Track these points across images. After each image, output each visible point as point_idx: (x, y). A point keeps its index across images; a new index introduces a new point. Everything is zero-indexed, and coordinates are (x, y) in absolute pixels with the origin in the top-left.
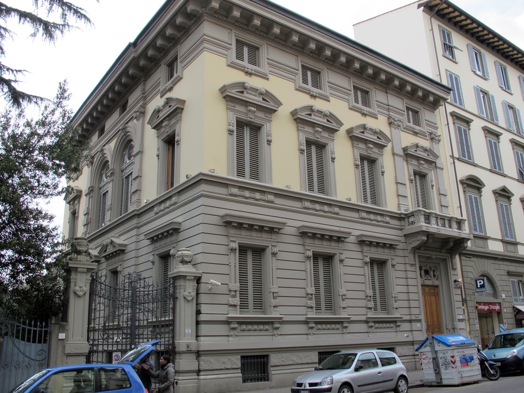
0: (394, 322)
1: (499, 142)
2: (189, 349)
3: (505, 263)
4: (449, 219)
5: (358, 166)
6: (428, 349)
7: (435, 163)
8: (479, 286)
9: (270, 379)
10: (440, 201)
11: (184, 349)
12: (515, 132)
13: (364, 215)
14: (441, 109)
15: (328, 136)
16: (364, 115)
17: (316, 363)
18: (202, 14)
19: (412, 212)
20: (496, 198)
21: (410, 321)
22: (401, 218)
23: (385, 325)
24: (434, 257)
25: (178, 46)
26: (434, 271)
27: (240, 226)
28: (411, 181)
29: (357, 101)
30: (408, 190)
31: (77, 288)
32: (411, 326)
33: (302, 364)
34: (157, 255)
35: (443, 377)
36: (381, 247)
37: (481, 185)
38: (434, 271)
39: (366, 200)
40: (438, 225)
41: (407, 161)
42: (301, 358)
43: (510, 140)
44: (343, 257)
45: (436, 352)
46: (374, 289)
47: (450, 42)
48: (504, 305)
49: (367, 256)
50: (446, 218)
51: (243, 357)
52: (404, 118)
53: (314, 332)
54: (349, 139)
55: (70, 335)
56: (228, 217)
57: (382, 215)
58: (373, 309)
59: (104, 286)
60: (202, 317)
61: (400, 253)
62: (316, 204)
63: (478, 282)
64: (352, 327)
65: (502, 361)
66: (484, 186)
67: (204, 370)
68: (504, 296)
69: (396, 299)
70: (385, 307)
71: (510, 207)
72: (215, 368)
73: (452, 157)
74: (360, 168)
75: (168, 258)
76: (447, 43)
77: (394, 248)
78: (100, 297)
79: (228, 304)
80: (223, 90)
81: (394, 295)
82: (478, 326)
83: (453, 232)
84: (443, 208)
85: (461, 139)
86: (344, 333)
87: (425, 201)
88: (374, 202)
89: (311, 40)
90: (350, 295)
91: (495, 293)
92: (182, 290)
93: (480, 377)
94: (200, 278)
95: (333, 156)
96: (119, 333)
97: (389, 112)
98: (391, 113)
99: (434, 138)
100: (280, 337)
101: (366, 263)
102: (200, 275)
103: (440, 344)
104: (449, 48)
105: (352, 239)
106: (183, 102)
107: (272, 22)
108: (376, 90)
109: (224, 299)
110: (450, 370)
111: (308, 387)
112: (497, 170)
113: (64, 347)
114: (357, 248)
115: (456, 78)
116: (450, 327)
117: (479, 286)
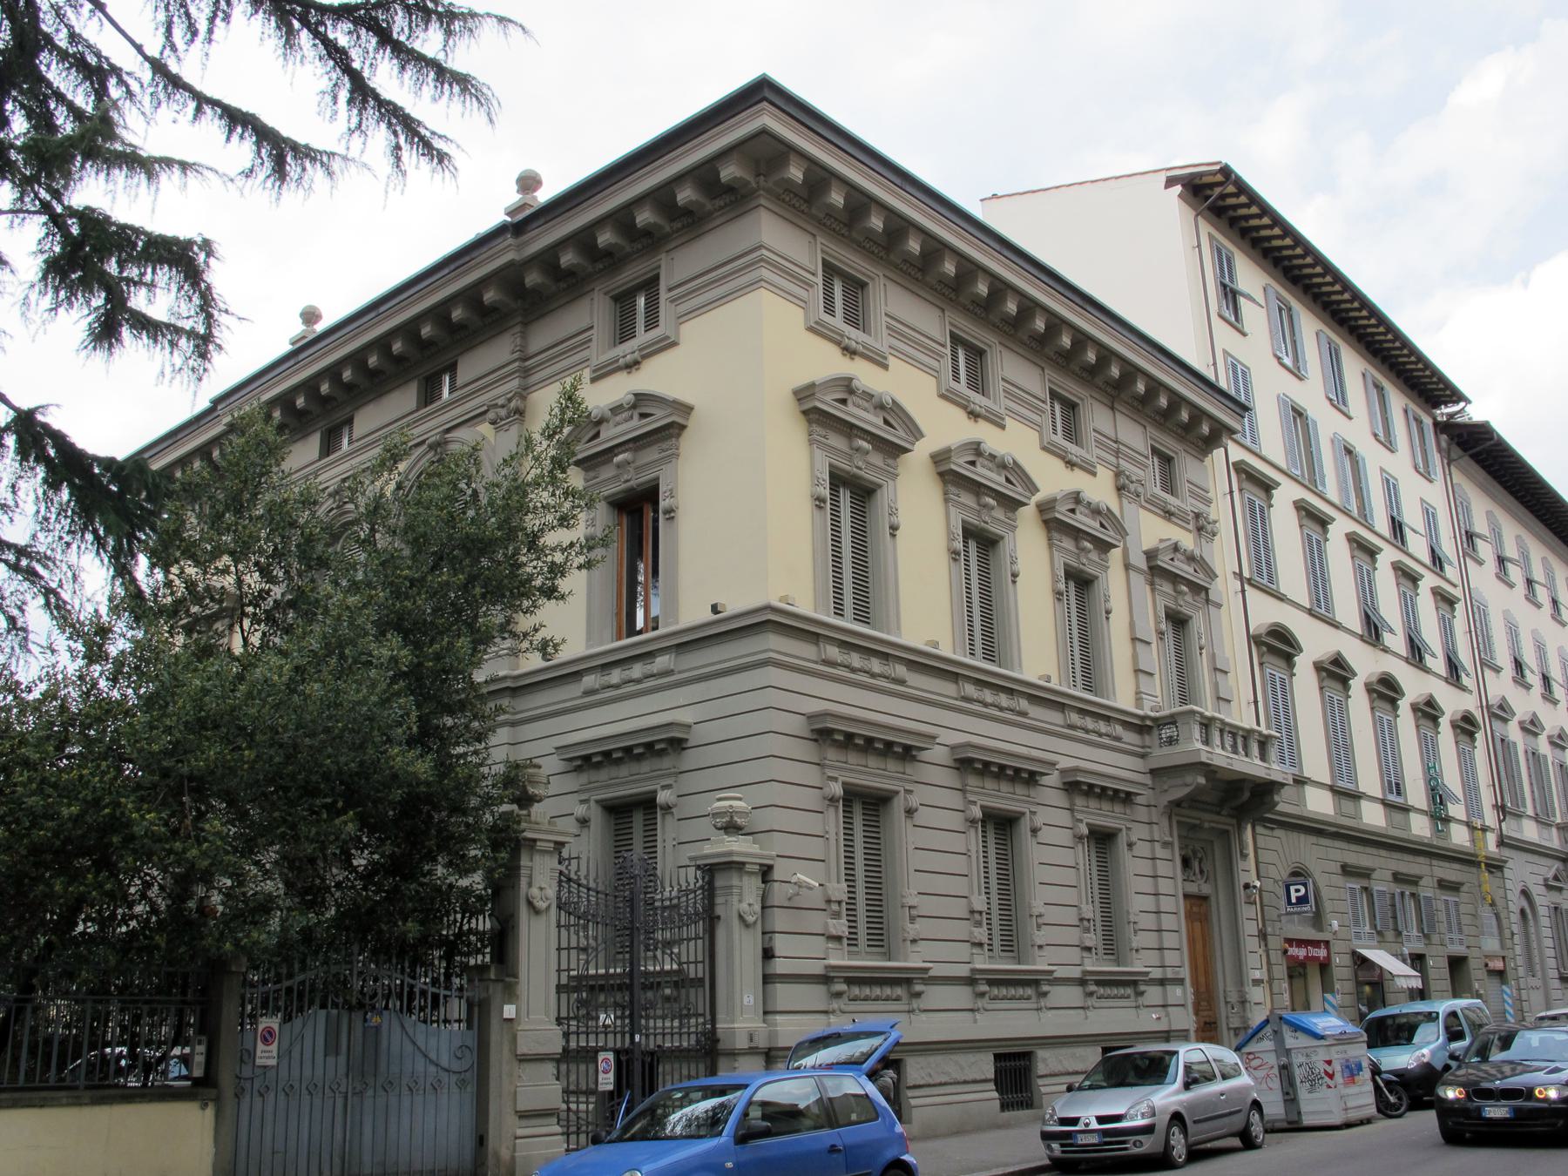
0: (1132, 983)
1: (1375, 569)
2: (753, 1045)
3: (1338, 844)
4: (1204, 721)
5: (824, 501)
6: (1268, 1044)
7: (1207, 590)
8: (1294, 901)
9: (1035, 1104)
10: (1216, 686)
12: (1355, 513)
13: (833, 652)
14: (1218, 453)
15: (1003, 518)
16: (849, 352)
17: (986, 1081)
18: (754, 191)
19: (1172, 716)
20: (1321, 680)
21: (1162, 982)
22: (1143, 727)
23: (877, 991)
24: (1206, 825)
25: (663, 256)
26: (1201, 861)
27: (848, 742)
28: (1161, 634)
29: (829, 309)
30: (1153, 657)
31: (535, 891)
32: (1165, 996)
33: (965, 1082)
34: (597, 802)
35: (1304, 1108)
36: (858, 749)
37: (1292, 646)
38: (1201, 861)
39: (839, 611)
40: (1223, 748)
41: (1152, 584)
42: (962, 1069)
43: (1347, 535)
44: (914, 801)
45: (1288, 1052)
46: (850, 879)
47: (1232, 280)
48: (1336, 947)
49: (835, 779)
50: (1241, 733)
51: (997, 1057)
52: (1148, 475)
53: (843, 1007)
54: (938, 477)
56: (829, 718)
57: (885, 657)
58: (845, 941)
60: (780, 966)
61: (1142, 813)
62: (873, 659)
63: (1292, 889)
64: (936, 996)
65: (1401, 1074)
66: (1301, 651)
68: (1335, 923)
69: (914, 912)
70: (879, 937)
71: (1291, 683)
73: (1239, 575)
74: (829, 511)
75: (631, 811)
76: (1227, 281)
77: (914, 759)
78: (570, 914)
80: (803, 394)
81: (1035, 912)
82: (1287, 996)
83: (1250, 765)
84: (1221, 703)
85: (1255, 530)
86: (978, 1010)
87: (1185, 687)
88: (863, 615)
89: (912, 230)
90: (927, 906)
91: (1318, 920)
92: (735, 899)
93: (1372, 1110)
94: (770, 867)
95: (894, 520)
97: (1117, 458)
98: (1121, 461)
99: (1202, 527)
100: (924, 1016)
101: (973, 821)
103: (1298, 1034)
104: (1230, 295)
105: (938, 754)
106: (687, 409)
107: (866, 200)
108: (1094, 402)
109: (816, 921)
110: (1323, 1092)
111: (1095, 1125)
112: (1323, 611)
113: (514, 1039)
114: (948, 777)
115: (1394, 485)
116: (1233, 997)
117: (1294, 901)
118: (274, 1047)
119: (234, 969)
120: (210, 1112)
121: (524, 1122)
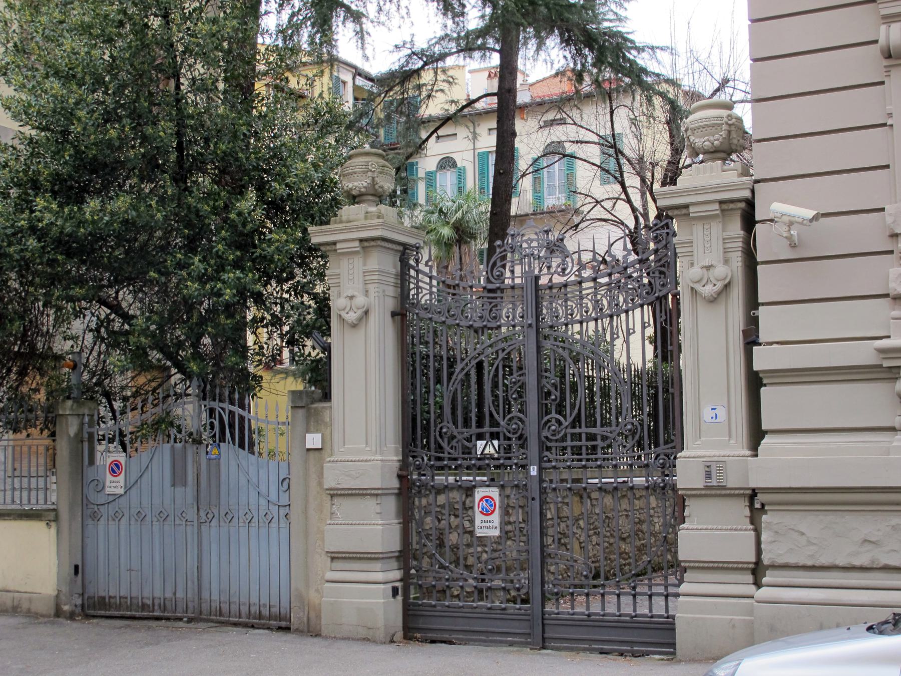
2: (714, 483)
11: (699, 482)
55: (337, 436)
59: (427, 280)
60: (763, 360)
67: (774, 567)
72: (824, 560)
79: (886, 296)
94: (750, 204)
96: (35, 474)
102: (747, 194)
118: (121, 478)
119: (61, 412)
120: (53, 530)
121: (338, 565)
